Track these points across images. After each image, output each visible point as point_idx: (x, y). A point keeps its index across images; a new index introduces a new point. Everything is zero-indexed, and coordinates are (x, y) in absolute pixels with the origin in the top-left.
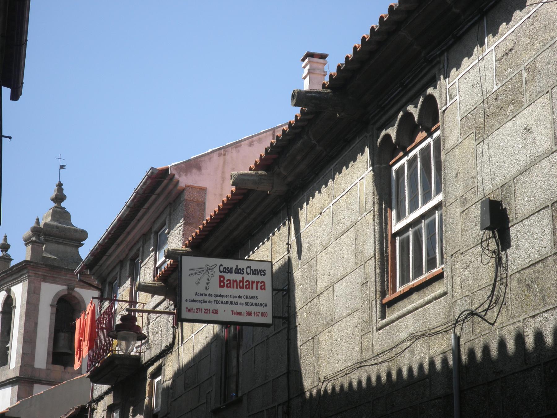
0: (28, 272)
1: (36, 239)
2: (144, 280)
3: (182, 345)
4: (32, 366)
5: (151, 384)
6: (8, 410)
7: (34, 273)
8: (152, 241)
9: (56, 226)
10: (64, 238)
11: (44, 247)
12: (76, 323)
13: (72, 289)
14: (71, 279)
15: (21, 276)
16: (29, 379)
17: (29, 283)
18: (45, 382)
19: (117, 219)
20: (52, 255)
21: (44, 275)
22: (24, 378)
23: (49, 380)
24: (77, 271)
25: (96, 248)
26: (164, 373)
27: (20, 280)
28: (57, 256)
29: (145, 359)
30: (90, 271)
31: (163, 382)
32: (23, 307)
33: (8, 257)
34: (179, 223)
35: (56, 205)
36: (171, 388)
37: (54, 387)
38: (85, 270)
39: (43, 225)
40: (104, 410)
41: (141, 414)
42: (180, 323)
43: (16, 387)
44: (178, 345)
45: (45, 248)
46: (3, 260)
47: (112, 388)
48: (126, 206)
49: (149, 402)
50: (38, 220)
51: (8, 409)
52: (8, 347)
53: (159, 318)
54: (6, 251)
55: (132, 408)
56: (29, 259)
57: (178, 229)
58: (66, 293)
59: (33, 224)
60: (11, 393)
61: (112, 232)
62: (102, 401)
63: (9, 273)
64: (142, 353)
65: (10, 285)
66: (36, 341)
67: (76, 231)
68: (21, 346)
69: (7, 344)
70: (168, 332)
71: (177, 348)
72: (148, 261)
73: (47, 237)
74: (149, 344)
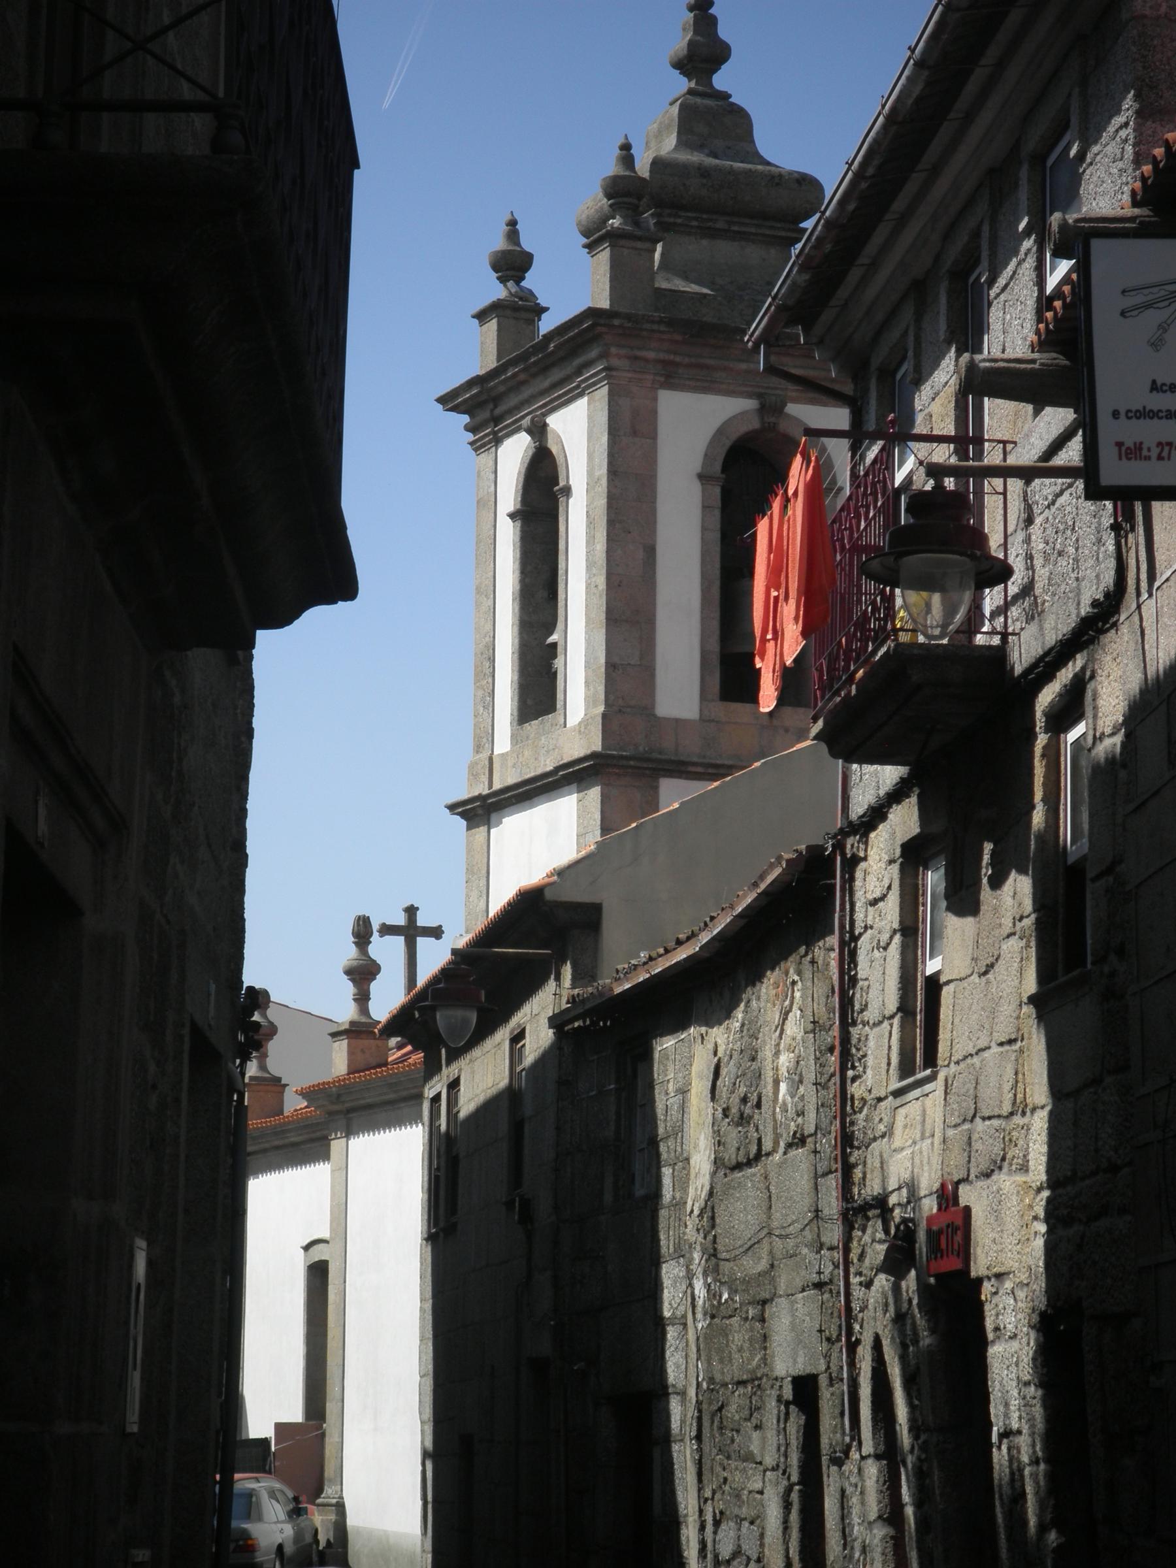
0: (603, 356)
1: (625, 223)
2: (1003, 352)
3: (1150, 595)
4: (647, 711)
5: (1053, 754)
7: (629, 358)
8: (1023, 194)
9: (699, 169)
11: (657, 256)
12: (755, 534)
15: (579, 372)
17: (611, 394)
18: (700, 770)
19: (881, 119)
20: (692, 282)
21: (664, 363)
22: (622, 757)
23: (713, 761)
24: (757, 333)
25: (817, 239)
26: (1095, 708)
27: (578, 387)
28: (711, 285)
29: (1023, 656)
30: (806, 331)
31: (1094, 743)
34: (1118, 112)
35: (693, 84)
36: (1124, 766)
37: (716, 784)
38: (787, 325)
39: (648, 166)
40: (891, 862)
41: (1022, 871)
42: (1138, 507)
43: (595, 793)
44: (1138, 594)
45: (662, 254)
46: (508, 312)
47: (911, 774)
48: (912, 62)
49: (1047, 821)
50: (626, 147)
52: (554, 645)
53: (1066, 495)
54: (519, 279)
55: (988, 847)
56: (604, 303)
57: (1118, 139)
58: (755, 424)
59: (610, 167)
60: (579, 817)
61: (870, 171)
62: (881, 827)
64: (1013, 634)
66: (654, 615)
67: (778, 180)
69: (551, 633)
70: (1103, 549)
71: (1134, 606)
72: (1014, 273)
73: (668, 211)
74: (1036, 598)
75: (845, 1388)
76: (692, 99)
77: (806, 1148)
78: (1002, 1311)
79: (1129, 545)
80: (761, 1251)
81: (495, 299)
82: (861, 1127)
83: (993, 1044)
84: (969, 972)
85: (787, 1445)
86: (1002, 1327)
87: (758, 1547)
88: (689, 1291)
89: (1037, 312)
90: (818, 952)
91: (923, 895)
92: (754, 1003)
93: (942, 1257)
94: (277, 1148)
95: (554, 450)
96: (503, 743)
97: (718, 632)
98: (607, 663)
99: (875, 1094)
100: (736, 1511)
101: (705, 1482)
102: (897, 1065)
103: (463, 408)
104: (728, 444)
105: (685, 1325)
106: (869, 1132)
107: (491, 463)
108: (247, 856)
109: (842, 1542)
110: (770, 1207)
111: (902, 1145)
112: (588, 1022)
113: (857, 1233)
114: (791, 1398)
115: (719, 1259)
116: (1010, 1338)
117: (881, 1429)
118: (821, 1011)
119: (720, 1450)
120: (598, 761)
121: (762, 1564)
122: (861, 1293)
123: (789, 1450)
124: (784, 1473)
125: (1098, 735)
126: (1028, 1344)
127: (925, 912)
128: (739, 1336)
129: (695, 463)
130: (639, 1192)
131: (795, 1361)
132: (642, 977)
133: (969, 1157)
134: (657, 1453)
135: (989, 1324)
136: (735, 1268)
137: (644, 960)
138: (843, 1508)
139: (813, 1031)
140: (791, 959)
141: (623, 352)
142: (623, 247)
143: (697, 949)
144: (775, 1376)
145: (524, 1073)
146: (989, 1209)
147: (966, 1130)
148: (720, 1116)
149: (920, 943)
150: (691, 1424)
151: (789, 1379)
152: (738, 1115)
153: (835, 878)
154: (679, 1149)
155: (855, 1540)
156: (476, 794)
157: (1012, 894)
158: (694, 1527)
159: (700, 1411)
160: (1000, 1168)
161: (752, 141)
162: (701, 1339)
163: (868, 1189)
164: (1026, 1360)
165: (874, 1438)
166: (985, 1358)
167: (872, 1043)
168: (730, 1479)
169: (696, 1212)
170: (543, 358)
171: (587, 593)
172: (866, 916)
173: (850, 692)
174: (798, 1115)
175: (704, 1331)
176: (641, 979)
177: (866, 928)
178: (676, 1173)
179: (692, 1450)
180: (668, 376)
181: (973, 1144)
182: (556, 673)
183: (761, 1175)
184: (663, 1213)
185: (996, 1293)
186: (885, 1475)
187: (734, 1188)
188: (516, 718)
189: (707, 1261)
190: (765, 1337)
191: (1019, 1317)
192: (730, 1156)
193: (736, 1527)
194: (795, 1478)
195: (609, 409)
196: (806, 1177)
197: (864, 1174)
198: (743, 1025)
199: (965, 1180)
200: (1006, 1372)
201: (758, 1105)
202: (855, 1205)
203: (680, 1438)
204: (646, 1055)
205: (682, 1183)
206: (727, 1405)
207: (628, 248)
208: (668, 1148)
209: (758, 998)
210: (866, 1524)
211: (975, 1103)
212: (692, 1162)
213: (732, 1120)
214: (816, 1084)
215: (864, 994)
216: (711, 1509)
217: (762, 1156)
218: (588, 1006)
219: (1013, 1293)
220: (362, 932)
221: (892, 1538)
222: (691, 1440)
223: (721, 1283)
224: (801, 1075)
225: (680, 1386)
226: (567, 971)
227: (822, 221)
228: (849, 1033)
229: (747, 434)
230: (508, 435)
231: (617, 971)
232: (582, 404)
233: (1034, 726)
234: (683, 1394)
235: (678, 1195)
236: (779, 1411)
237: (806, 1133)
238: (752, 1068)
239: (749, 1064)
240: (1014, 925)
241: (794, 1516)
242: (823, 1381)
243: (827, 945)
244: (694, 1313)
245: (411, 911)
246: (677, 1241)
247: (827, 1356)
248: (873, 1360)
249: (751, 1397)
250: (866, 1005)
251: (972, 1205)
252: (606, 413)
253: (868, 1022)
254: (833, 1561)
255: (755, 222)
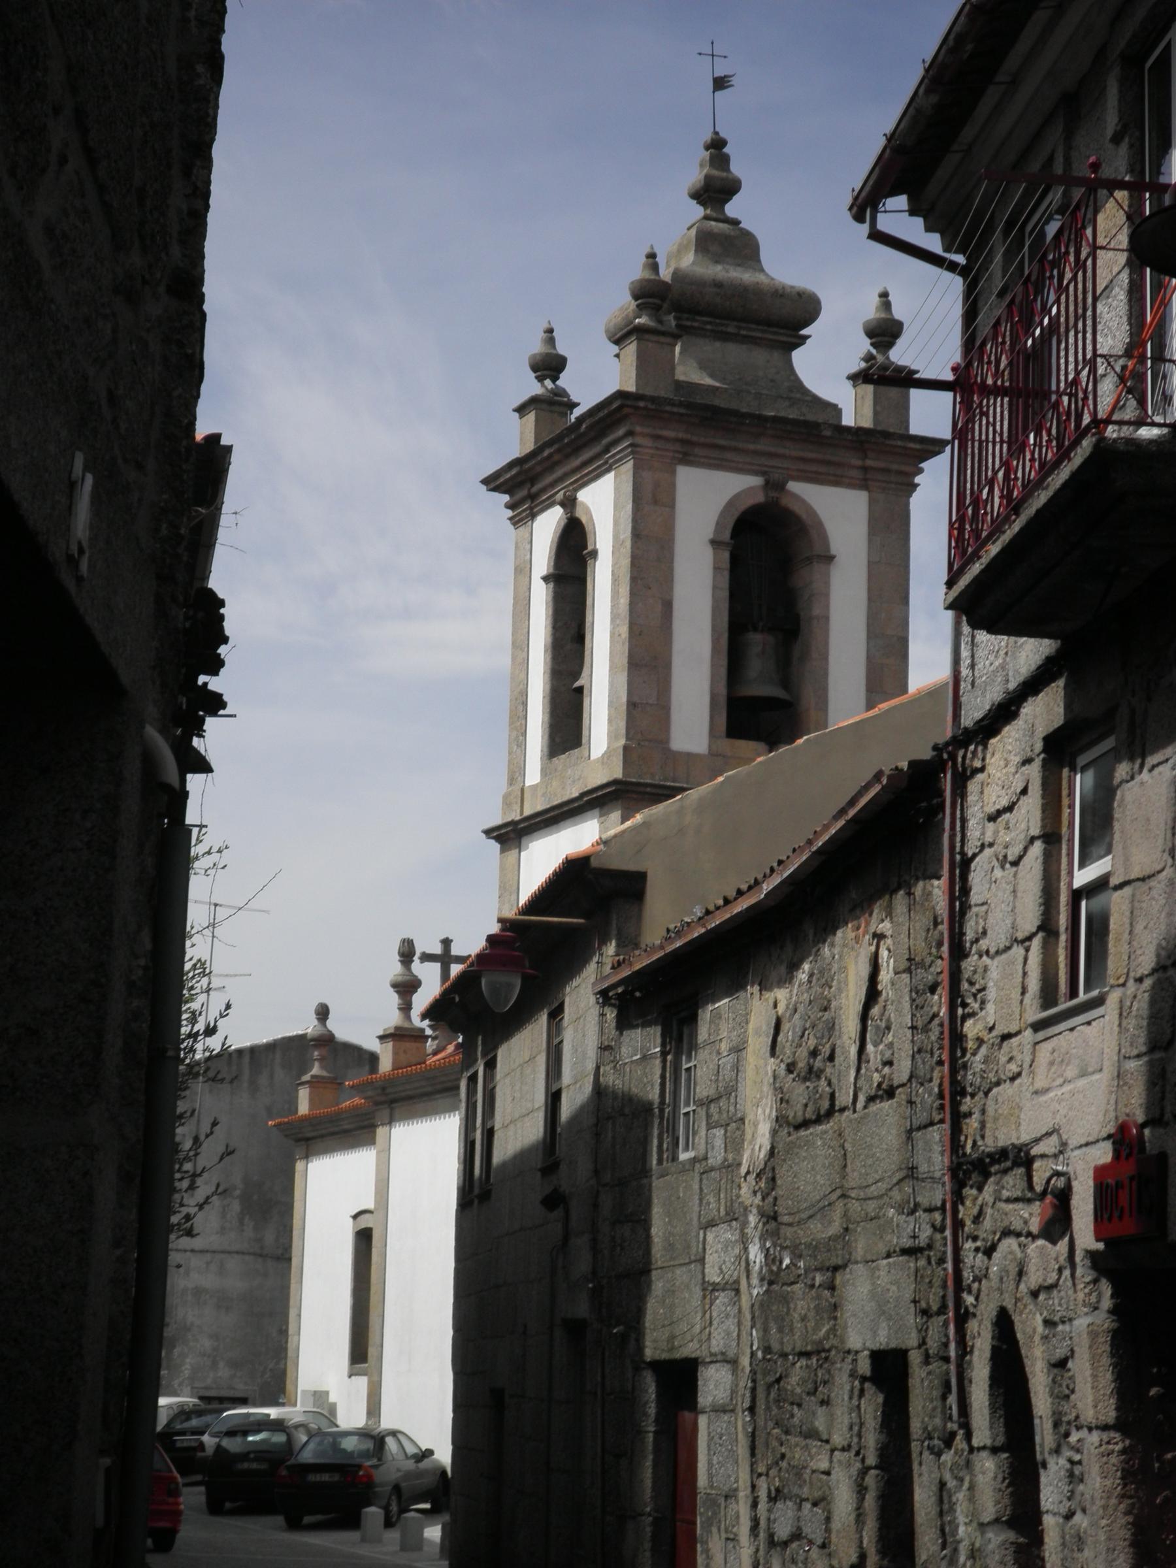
13: (780, 486)
15: (607, 450)
21: (683, 442)
27: (606, 462)
32: (623, 550)
33: (560, 396)
35: (708, 211)
40: (1027, 761)
46: (544, 406)
54: (555, 379)
56: (631, 387)
58: (760, 498)
59: (637, 271)
65: (572, 484)
67: (780, 294)
68: (623, 678)
73: (686, 315)
77: (895, 1100)
80: (833, 1214)
81: (533, 394)
82: (978, 1070)
85: (861, 1425)
87: (823, 1532)
94: (333, 1134)
95: (584, 520)
96: (533, 776)
98: (628, 701)
99: (1000, 1029)
100: (795, 1490)
101: (759, 1456)
104: (736, 515)
105: (737, 1291)
107: (527, 535)
108: (203, 316)
109: (940, 1541)
110: (845, 1166)
111: (1047, 1086)
114: (868, 1374)
115: (782, 1224)
117: (1000, 1417)
118: (920, 946)
119: (777, 1424)
120: (619, 787)
123: (864, 1430)
124: (858, 1453)
127: (1072, 815)
128: (802, 1303)
129: (709, 532)
131: (875, 1334)
136: (799, 1231)
142: (647, 340)
143: (762, 896)
144: (847, 1348)
150: (744, 1395)
151: (866, 1353)
152: (806, 1069)
154: (732, 1108)
156: (510, 819)
158: (746, 1503)
159: (754, 1381)
162: (756, 1307)
168: (788, 1455)
170: (575, 439)
172: (983, 834)
175: (760, 1298)
176: (696, 935)
178: (728, 1134)
180: (685, 454)
183: (835, 1132)
186: (1004, 1471)
187: (800, 1147)
188: (546, 754)
189: (764, 1224)
192: (796, 1112)
193: (795, 1507)
194: (871, 1460)
195: (634, 481)
196: (894, 1132)
197: (983, 1125)
198: (811, 975)
203: (731, 1407)
206: (786, 1376)
207: (652, 342)
208: (720, 1108)
210: (975, 1524)
213: (798, 1075)
215: (981, 920)
217: (836, 1111)
220: (407, 953)
222: (743, 1412)
224: (888, 1020)
238: (824, 1019)
239: (821, 1014)
242: (915, 1357)
244: (748, 1277)
245: (447, 943)
246: (728, 1204)
248: (993, 1338)
249: (816, 1370)
250: (984, 933)
252: (631, 484)
254: (926, 1561)
255: (760, 327)
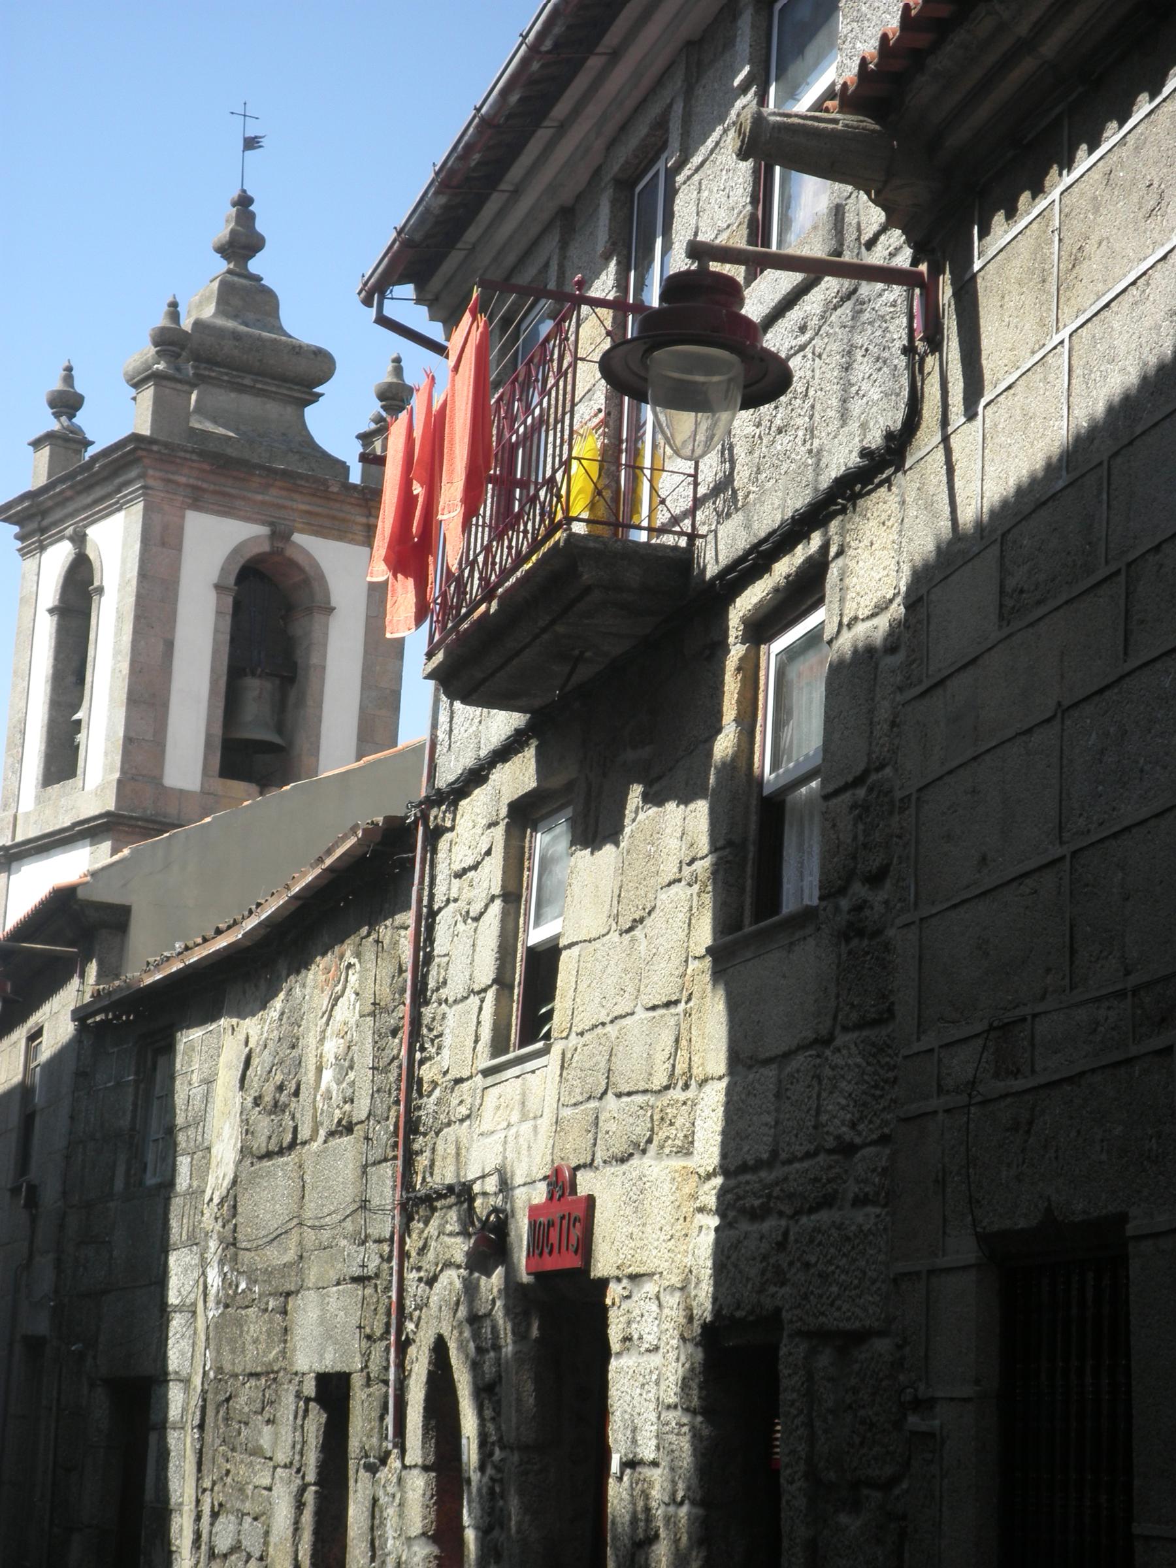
0: (142, 476)
1: (168, 367)
3: (971, 415)
4: (156, 780)
5: (750, 670)
6: (89, 878)
10: (258, 374)
14: (281, 501)
15: (119, 490)
16: (146, 820)
21: (195, 488)
22: (132, 818)
27: (117, 502)
28: (236, 431)
32: (129, 589)
35: (232, 266)
44: (945, 422)
46: (60, 442)
50: (174, 305)
51: (85, 876)
52: (79, 722)
54: (71, 416)
56: (145, 430)
58: (266, 547)
59: (160, 320)
63: (81, 482)
66: (168, 700)
67: (298, 350)
72: (717, 144)
73: (204, 365)
74: (734, 492)
75: (391, 1391)
76: (229, 277)
78: (638, 1319)
79: (927, 370)
83: (639, 1009)
84: (606, 931)
85: (304, 1443)
86: (636, 1337)
88: (201, 1280)
89: (754, 172)
90: (385, 931)
91: (529, 859)
92: (297, 991)
93: (551, 1253)
95: (92, 556)
97: (221, 719)
100: (238, 1505)
102: (489, 1042)
103: (14, 519)
105: (194, 1313)
106: (442, 1117)
107: (35, 567)
110: (303, 1197)
112: (110, 1016)
113: (417, 1225)
114: (313, 1395)
116: (648, 1351)
121: (264, 1563)
122: (420, 1290)
124: (298, 1471)
125: (845, 621)
126: (678, 1360)
127: (530, 877)
128: (255, 1326)
129: (213, 576)
130: (151, 1180)
131: (321, 1357)
132: (176, 966)
133: (595, 1139)
134: (153, 1438)
135: (615, 1334)
137: (179, 950)
138: (373, 1517)
139: (373, 1014)
140: (348, 941)
141: (158, 474)
145: (38, 1069)
146: (624, 1198)
147: (591, 1109)
148: (250, 1105)
149: (522, 911)
151: (312, 1375)
152: (272, 1103)
153: (414, 849)
154: (199, 1138)
155: (388, 1555)
157: (679, 835)
159: (204, 1400)
160: (644, 1152)
161: (278, 318)
163: (437, 1178)
164: (672, 1378)
165: (423, 1447)
166: (605, 1371)
167: (450, 1021)
169: (216, 1200)
171: (112, 677)
172: (449, 889)
173: (488, 609)
174: (345, 1102)
176: (174, 969)
177: (448, 901)
179: (193, 1439)
180: (196, 500)
181: (601, 1124)
182: (78, 747)
184: (176, 1203)
185: (628, 1297)
187: (262, 1177)
189: (224, 1250)
190: (286, 1330)
191: (664, 1327)
192: (260, 1143)
194: (311, 1477)
196: (351, 1166)
198: (282, 1014)
199: (589, 1165)
200: (638, 1391)
201: (296, 1093)
202: (419, 1195)
204: (169, 1048)
205: (201, 1171)
206: (236, 1396)
209: (304, 986)
210: (403, 1538)
211: (608, 1078)
212: (214, 1151)
214: (373, 1068)
216: (209, 1500)
218: (115, 997)
219: (658, 1298)
221: (436, 1557)
223: (239, 1273)
224: (352, 1060)
225: (184, 1374)
226: (92, 969)
227: (477, 120)
228: (420, 1014)
229: (259, 555)
230: (52, 544)
231: (148, 964)
232: (119, 519)
233: (726, 636)
234: (186, 1382)
235: (195, 1184)
236: (297, 1407)
237: (355, 1120)
240: (680, 870)
241: (308, 1517)
242: (357, 1381)
243: (396, 923)
244: (205, 1302)
247: (366, 1356)
248: (429, 1363)
250: (445, 983)
251: (596, 1195)
253: (446, 1001)
